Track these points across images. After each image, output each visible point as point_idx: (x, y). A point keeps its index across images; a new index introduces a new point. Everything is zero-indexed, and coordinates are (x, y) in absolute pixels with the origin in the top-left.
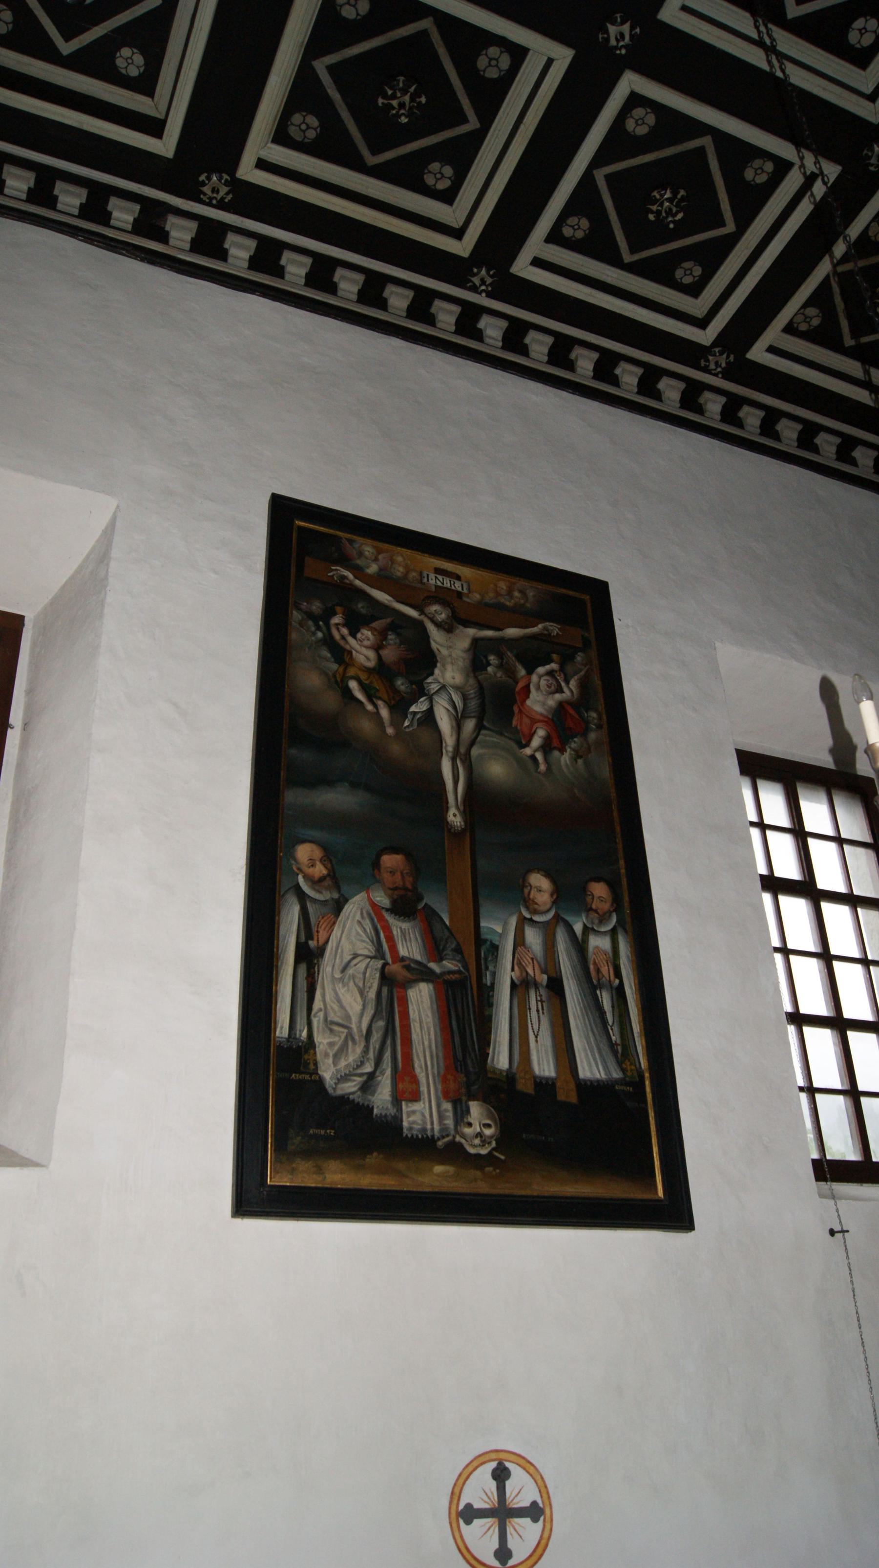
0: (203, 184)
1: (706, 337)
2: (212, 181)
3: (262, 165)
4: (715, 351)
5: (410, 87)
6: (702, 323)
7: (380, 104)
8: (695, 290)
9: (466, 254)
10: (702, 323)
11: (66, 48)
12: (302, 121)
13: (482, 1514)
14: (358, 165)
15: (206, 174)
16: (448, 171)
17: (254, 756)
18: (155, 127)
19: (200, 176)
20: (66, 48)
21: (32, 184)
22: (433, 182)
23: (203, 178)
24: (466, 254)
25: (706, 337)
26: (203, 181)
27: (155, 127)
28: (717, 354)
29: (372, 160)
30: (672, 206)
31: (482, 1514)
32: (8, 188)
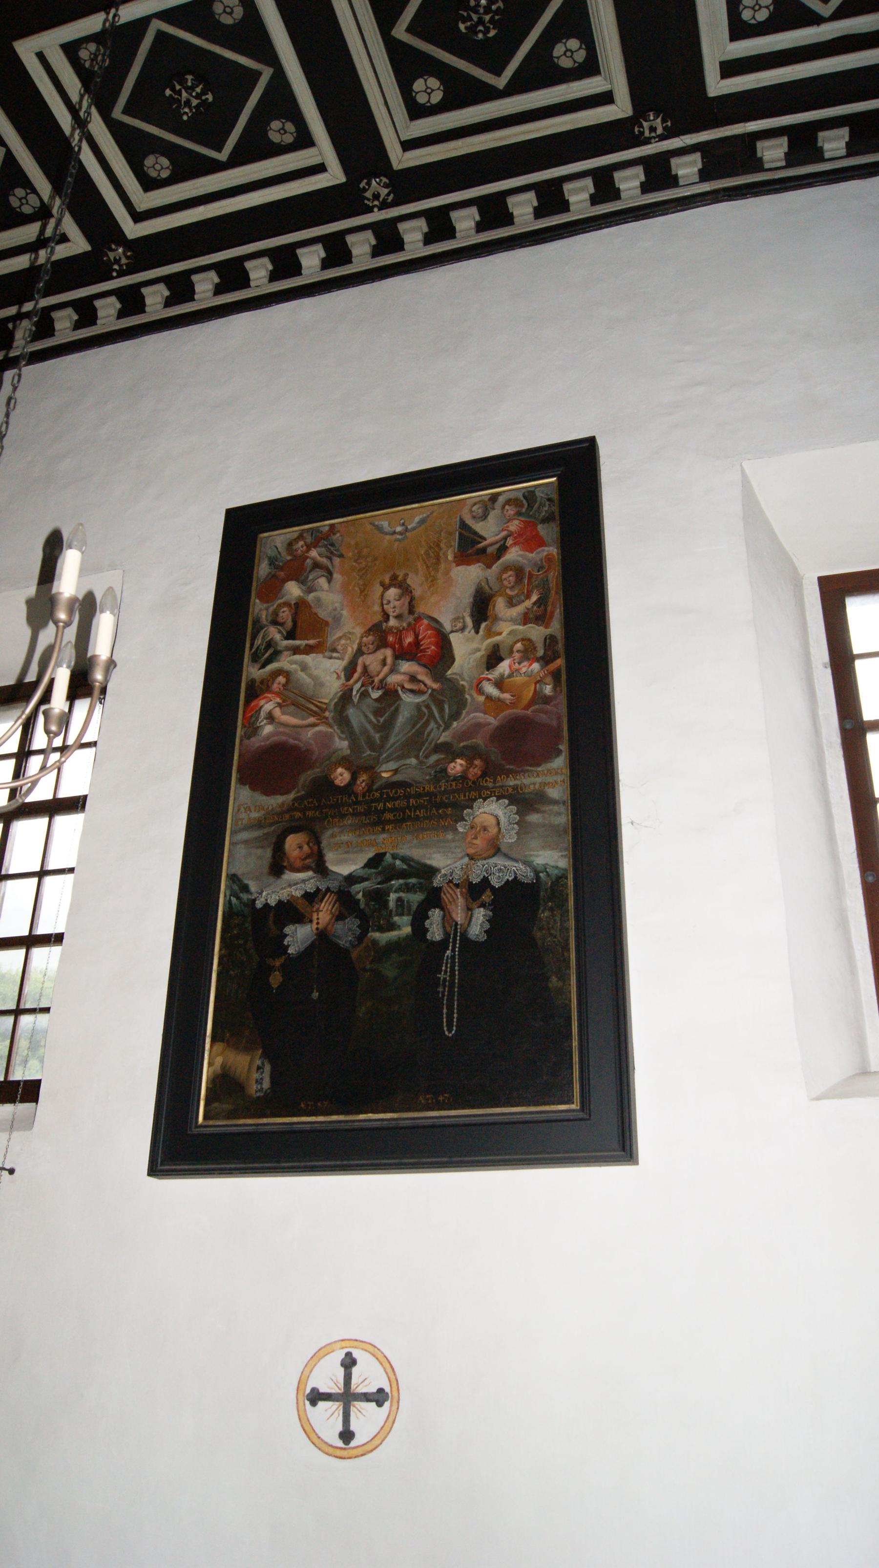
0: (365, 190)
1: (132, 230)
2: (372, 186)
3: (408, 145)
4: (667, 121)
5: (197, 86)
6: (138, 217)
7: (464, 30)
8: (149, 184)
9: (396, 166)
10: (138, 217)
11: (223, 156)
12: (155, 162)
13: (366, 1397)
14: (492, 94)
15: (365, 181)
16: (573, 44)
17: (611, 685)
18: (606, 98)
19: (360, 183)
20: (501, 82)
21: (642, 178)
22: (426, 100)
23: (363, 184)
24: (396, 166)
25: (132, 230)
26: (364, 188)
27: (606, 98)
28: (382, 184)
29: (223, 156)
30: (191, 98)
31: (366, 1397)
32: (827, 151)
